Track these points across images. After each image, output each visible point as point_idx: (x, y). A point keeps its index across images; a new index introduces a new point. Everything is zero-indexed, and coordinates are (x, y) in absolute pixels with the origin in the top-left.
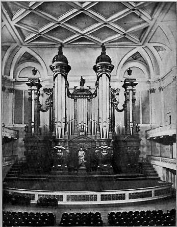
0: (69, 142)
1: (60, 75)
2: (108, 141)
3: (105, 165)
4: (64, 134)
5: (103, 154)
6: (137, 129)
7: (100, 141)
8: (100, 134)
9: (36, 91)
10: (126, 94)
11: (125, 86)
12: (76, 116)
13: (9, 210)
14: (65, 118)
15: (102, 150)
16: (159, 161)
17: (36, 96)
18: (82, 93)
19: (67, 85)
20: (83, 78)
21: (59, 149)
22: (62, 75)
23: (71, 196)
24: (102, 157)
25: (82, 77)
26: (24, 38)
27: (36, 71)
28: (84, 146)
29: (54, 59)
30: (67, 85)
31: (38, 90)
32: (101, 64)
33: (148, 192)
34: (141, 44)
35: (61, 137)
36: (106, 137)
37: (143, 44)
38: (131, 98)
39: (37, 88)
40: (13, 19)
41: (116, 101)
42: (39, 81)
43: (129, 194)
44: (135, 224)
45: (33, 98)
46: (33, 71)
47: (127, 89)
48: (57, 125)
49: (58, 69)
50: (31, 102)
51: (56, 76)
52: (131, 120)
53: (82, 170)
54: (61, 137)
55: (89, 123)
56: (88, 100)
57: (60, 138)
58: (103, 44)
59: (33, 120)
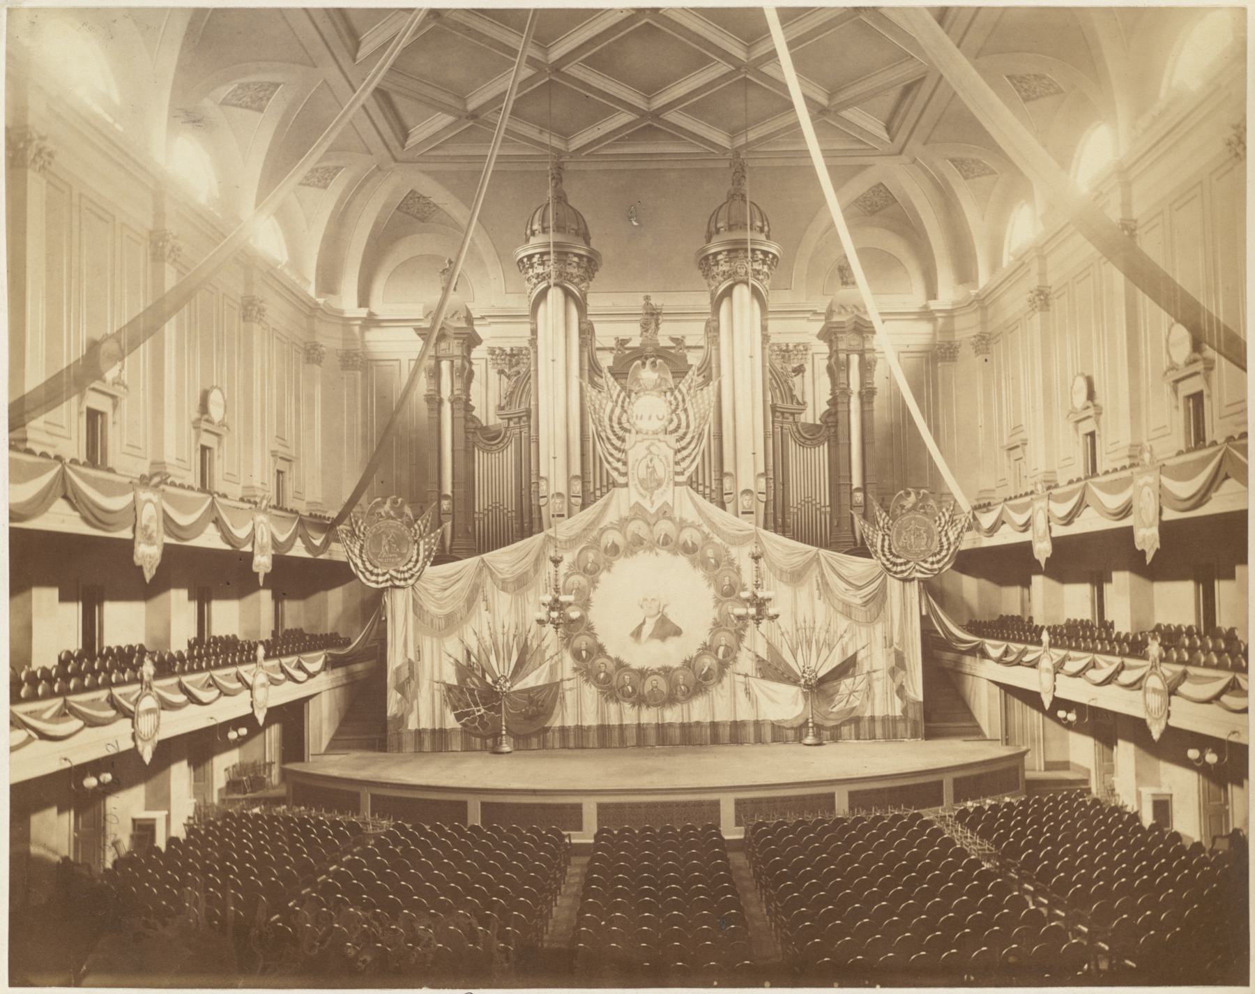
1: (555, 295)
10: (836, 370)
11: (829, 334)
13: (769, 738)
17: (458, 385)
19: (586, 333)
22: (568, 293)
23: (849, 411)
26: (405, 133)
30: (586, 333)
31: (467, 358)
33: (819, 796)
38: (855, 385)
40: (363, 53)
41: (793, 397)
42: (469, 319)
44: (12, 428)
45: (446, 393)
47: (842, 345)
50: (439, 412)
51: (543, 295)
52: (856, 482)
58: (737, 153)
59: (448, 490)
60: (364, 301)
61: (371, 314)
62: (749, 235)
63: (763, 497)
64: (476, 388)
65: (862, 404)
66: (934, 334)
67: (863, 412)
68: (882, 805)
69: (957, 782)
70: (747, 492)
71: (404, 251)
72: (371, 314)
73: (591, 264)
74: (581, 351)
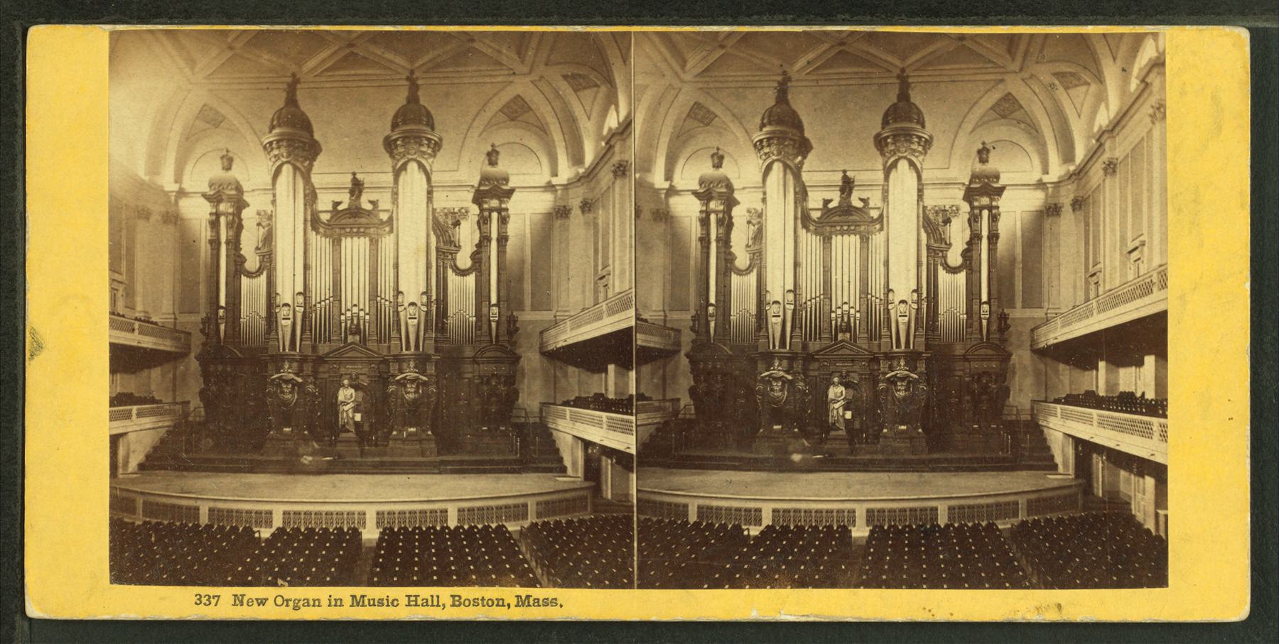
0: (805, 360)
2: (422, 361)
3: (903, 427)
4: (301, 340)
5: (407, 397)
6: (1003, 322)
7: (889, 357)
8: (891, 337)
9: (721, 215)
12: (827, 283)
14: (795, 291)
15: (405, 385)
16: (600, 424)
18: (844, 216)
20: (359, 176)
21: (776, 379)
24: (403, 404)
25: (354, 174)
27: (721, 158)
28: (357, 376)
29: (396, 117)
32: (404, 132)
33: (1008, 504)
34: (526, 70)
35: (783, 344)
36: (417, 347)
37: (1021, 70)
39: (231, 210)
43: (774, 511)
45: (223, 238)
46: (222, 158)
48: (772, 310)
49: (774, 148)
53: (347, 441)
54: (783, 344)
55: (373, 311)
56: (371, 240)
57: (404, 352)
58: (903, 70)
60: (669, 177)
61: (671, 186)
62: (914, 126)
63: (915, 306)
64: (245, 236)
65: (989, 244)
66: (555, 201)
67: (989, 250)
68: (566, 511)
69: (1029, 502)
70: (903, 302)
71: (199, 150)
72: (671, 186)
73: (804, 147)
74: (796, 207)
